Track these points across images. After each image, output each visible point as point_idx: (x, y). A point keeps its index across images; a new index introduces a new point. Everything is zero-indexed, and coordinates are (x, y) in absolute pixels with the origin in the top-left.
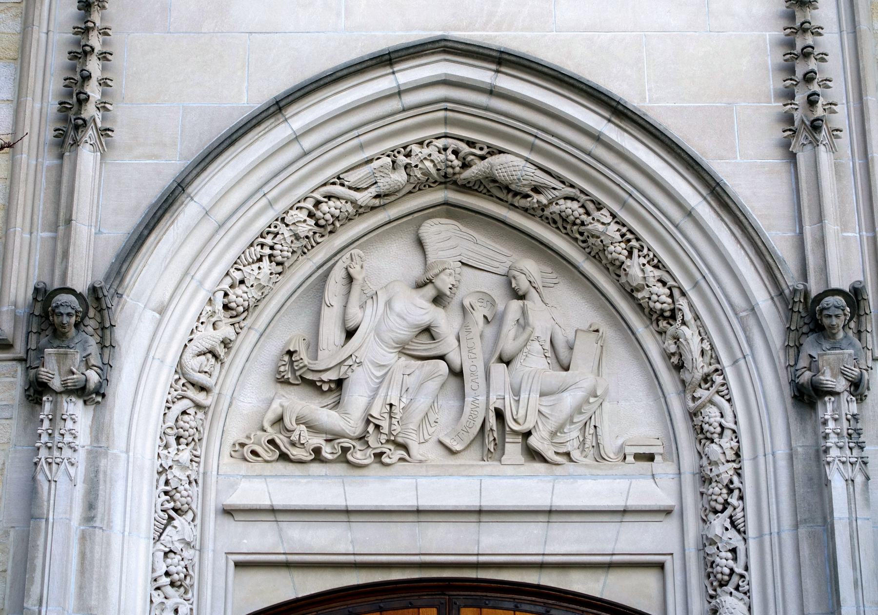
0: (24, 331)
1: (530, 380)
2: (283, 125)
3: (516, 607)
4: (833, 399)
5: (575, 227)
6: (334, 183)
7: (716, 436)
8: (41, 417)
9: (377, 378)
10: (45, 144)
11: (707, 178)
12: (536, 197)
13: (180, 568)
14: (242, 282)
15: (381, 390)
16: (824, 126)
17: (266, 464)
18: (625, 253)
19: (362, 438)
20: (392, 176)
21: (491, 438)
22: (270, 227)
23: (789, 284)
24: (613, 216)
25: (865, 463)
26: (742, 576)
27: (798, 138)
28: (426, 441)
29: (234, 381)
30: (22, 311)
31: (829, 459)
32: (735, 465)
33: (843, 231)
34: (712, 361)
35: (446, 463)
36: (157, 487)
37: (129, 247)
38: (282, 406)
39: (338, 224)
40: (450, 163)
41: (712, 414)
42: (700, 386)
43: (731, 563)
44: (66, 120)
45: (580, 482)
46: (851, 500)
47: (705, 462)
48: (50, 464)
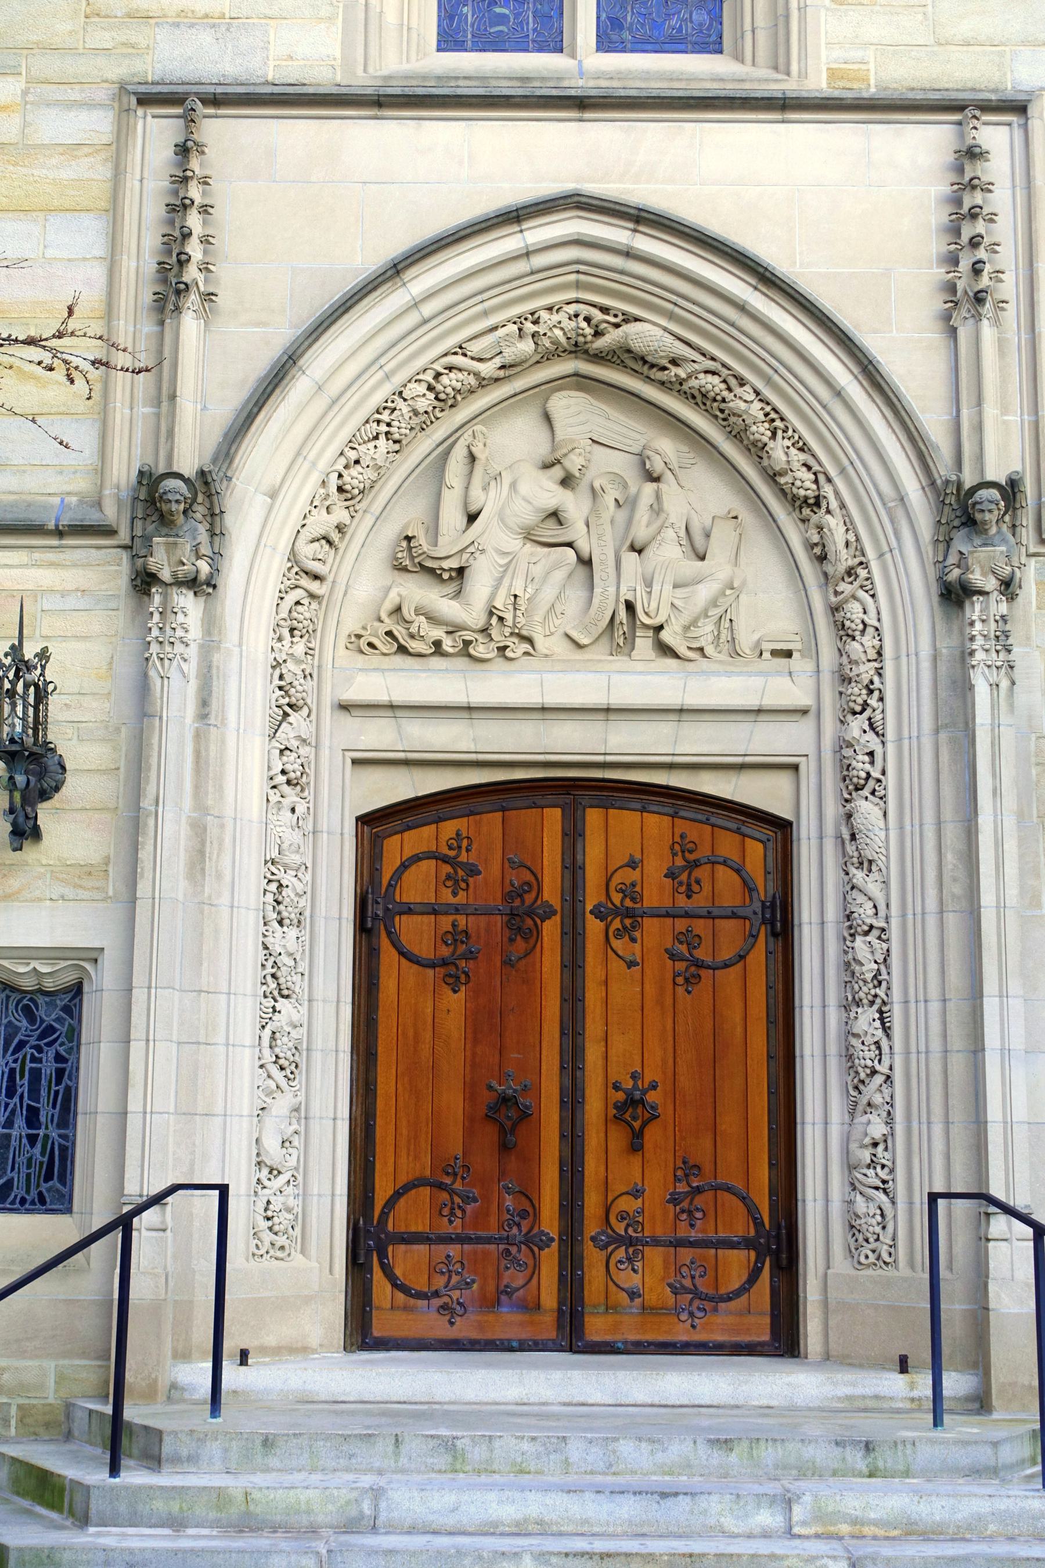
0: (129, 516)
1: (663, 571)
2: (401, 290)
3: (644, 807)
4: (981, 598)
5: (715, 404)
6: (455, 353)
7: (857, 633)
8: (151, 609)
9: (501, 566)
10: (143, 308)
11: (860, 355)
12: (674, 370)
13: (296, 766)
14: (357, 462)
15: (505, 580)
16: (989, 298)
17: (383, 657)
18: (769, 433)
19: (484, 631)
20: (518, 345)
21: (621, 632)
22: (386, 402)
23: (942, 473)
24: (757, 393)
25: (1012, 667)
26: (879, 781)
27: (960, 310)
28: (552, 634)
29: (349, 568)
30: (124, 494)
31: (974, 663)
32: (876, 665)
33: (1003, 414)
34: (857, 553)
35: (573, 657)
36: (271, 682)
37: (237, 426)
38: (400, 595)
39: (459, 398)
40: (581, 332)
41: (854, 610)
42: (843, 579)
43: (868, 767)
44: (165, 281)
45: (713, 679)
46: (994, 706)
47: (845, 660)
48: (162, 659)
